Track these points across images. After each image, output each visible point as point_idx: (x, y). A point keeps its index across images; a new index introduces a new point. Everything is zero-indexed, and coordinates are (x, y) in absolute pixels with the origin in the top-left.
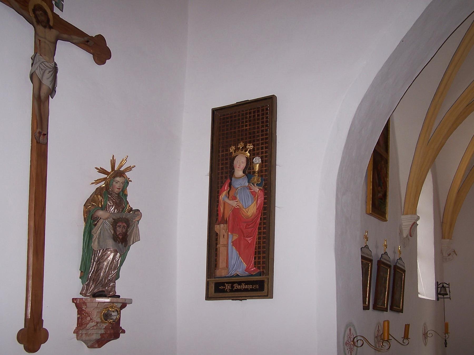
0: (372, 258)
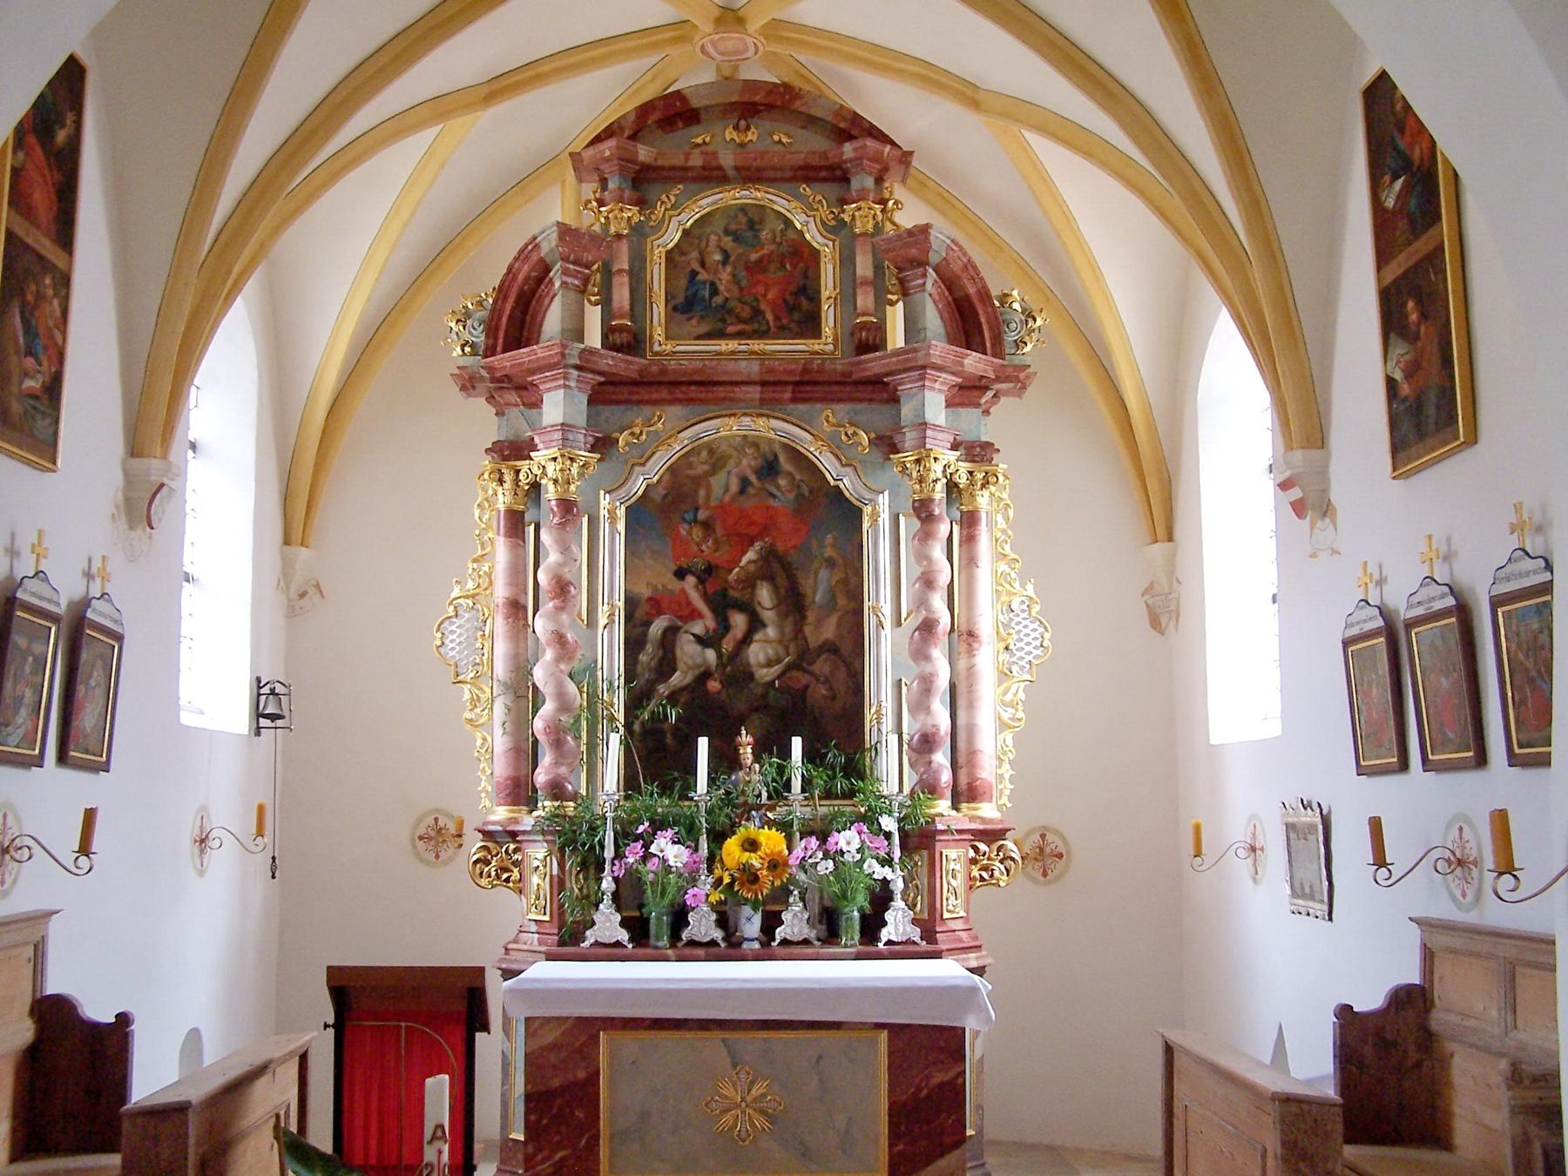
0: (121, 631)
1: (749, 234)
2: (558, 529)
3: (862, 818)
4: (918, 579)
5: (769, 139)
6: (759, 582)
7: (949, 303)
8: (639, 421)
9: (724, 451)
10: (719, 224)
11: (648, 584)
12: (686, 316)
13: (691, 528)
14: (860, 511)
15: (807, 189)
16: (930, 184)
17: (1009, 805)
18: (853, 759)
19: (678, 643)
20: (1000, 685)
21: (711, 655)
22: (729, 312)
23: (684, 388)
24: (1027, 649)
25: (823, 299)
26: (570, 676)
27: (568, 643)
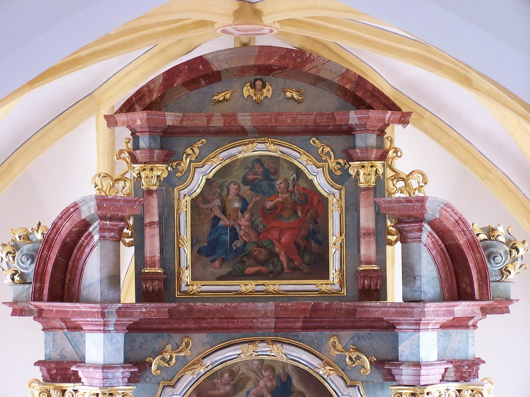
1: (265, 183)
5: (283, 94)
7: (442, 249)
8: (169, 347)
9: (243, 373)
10: (238, 174)
12: (210, 259)
15: (317, 141)
16: (427, 115)
22: (249, 255)
25: (331, 245)
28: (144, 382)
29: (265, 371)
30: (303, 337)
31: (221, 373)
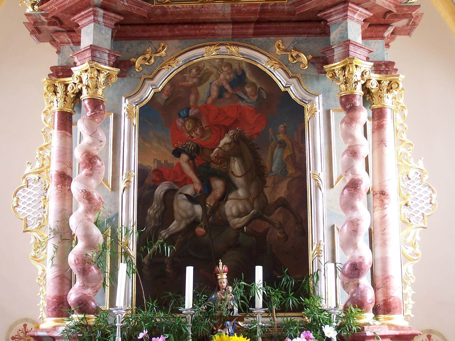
2: (89, 119)
3: (308, 327)
4: (346, 151)
6: (232, 158)
9: (208, 69)
11: (154, 160)
13: (185, 121)
14: (303, 108)
17: (412, 316)
18: (300, 283)
19: (175, 201)
20: (402, 230)
21: (198, 209)
23: (180, 27)
24: (421, 205)
26: (96, 223)
27: (95, 199)
28: (129, 77)
29: (224, 67)
30: (254, 42)
31: (189, 69)
